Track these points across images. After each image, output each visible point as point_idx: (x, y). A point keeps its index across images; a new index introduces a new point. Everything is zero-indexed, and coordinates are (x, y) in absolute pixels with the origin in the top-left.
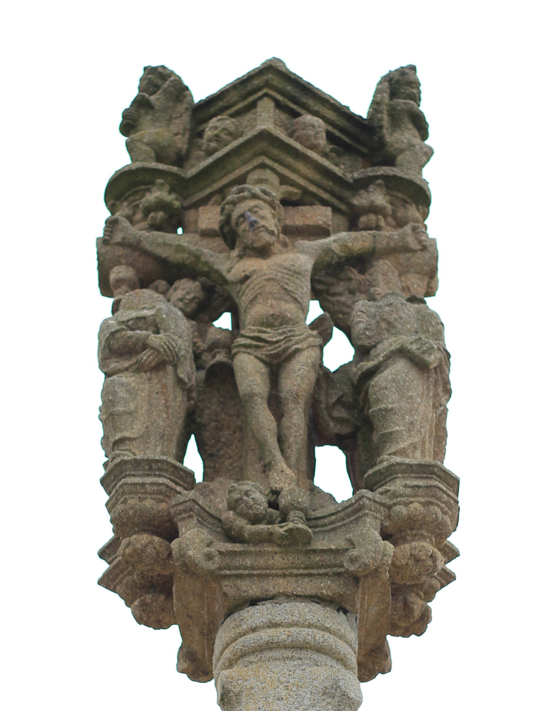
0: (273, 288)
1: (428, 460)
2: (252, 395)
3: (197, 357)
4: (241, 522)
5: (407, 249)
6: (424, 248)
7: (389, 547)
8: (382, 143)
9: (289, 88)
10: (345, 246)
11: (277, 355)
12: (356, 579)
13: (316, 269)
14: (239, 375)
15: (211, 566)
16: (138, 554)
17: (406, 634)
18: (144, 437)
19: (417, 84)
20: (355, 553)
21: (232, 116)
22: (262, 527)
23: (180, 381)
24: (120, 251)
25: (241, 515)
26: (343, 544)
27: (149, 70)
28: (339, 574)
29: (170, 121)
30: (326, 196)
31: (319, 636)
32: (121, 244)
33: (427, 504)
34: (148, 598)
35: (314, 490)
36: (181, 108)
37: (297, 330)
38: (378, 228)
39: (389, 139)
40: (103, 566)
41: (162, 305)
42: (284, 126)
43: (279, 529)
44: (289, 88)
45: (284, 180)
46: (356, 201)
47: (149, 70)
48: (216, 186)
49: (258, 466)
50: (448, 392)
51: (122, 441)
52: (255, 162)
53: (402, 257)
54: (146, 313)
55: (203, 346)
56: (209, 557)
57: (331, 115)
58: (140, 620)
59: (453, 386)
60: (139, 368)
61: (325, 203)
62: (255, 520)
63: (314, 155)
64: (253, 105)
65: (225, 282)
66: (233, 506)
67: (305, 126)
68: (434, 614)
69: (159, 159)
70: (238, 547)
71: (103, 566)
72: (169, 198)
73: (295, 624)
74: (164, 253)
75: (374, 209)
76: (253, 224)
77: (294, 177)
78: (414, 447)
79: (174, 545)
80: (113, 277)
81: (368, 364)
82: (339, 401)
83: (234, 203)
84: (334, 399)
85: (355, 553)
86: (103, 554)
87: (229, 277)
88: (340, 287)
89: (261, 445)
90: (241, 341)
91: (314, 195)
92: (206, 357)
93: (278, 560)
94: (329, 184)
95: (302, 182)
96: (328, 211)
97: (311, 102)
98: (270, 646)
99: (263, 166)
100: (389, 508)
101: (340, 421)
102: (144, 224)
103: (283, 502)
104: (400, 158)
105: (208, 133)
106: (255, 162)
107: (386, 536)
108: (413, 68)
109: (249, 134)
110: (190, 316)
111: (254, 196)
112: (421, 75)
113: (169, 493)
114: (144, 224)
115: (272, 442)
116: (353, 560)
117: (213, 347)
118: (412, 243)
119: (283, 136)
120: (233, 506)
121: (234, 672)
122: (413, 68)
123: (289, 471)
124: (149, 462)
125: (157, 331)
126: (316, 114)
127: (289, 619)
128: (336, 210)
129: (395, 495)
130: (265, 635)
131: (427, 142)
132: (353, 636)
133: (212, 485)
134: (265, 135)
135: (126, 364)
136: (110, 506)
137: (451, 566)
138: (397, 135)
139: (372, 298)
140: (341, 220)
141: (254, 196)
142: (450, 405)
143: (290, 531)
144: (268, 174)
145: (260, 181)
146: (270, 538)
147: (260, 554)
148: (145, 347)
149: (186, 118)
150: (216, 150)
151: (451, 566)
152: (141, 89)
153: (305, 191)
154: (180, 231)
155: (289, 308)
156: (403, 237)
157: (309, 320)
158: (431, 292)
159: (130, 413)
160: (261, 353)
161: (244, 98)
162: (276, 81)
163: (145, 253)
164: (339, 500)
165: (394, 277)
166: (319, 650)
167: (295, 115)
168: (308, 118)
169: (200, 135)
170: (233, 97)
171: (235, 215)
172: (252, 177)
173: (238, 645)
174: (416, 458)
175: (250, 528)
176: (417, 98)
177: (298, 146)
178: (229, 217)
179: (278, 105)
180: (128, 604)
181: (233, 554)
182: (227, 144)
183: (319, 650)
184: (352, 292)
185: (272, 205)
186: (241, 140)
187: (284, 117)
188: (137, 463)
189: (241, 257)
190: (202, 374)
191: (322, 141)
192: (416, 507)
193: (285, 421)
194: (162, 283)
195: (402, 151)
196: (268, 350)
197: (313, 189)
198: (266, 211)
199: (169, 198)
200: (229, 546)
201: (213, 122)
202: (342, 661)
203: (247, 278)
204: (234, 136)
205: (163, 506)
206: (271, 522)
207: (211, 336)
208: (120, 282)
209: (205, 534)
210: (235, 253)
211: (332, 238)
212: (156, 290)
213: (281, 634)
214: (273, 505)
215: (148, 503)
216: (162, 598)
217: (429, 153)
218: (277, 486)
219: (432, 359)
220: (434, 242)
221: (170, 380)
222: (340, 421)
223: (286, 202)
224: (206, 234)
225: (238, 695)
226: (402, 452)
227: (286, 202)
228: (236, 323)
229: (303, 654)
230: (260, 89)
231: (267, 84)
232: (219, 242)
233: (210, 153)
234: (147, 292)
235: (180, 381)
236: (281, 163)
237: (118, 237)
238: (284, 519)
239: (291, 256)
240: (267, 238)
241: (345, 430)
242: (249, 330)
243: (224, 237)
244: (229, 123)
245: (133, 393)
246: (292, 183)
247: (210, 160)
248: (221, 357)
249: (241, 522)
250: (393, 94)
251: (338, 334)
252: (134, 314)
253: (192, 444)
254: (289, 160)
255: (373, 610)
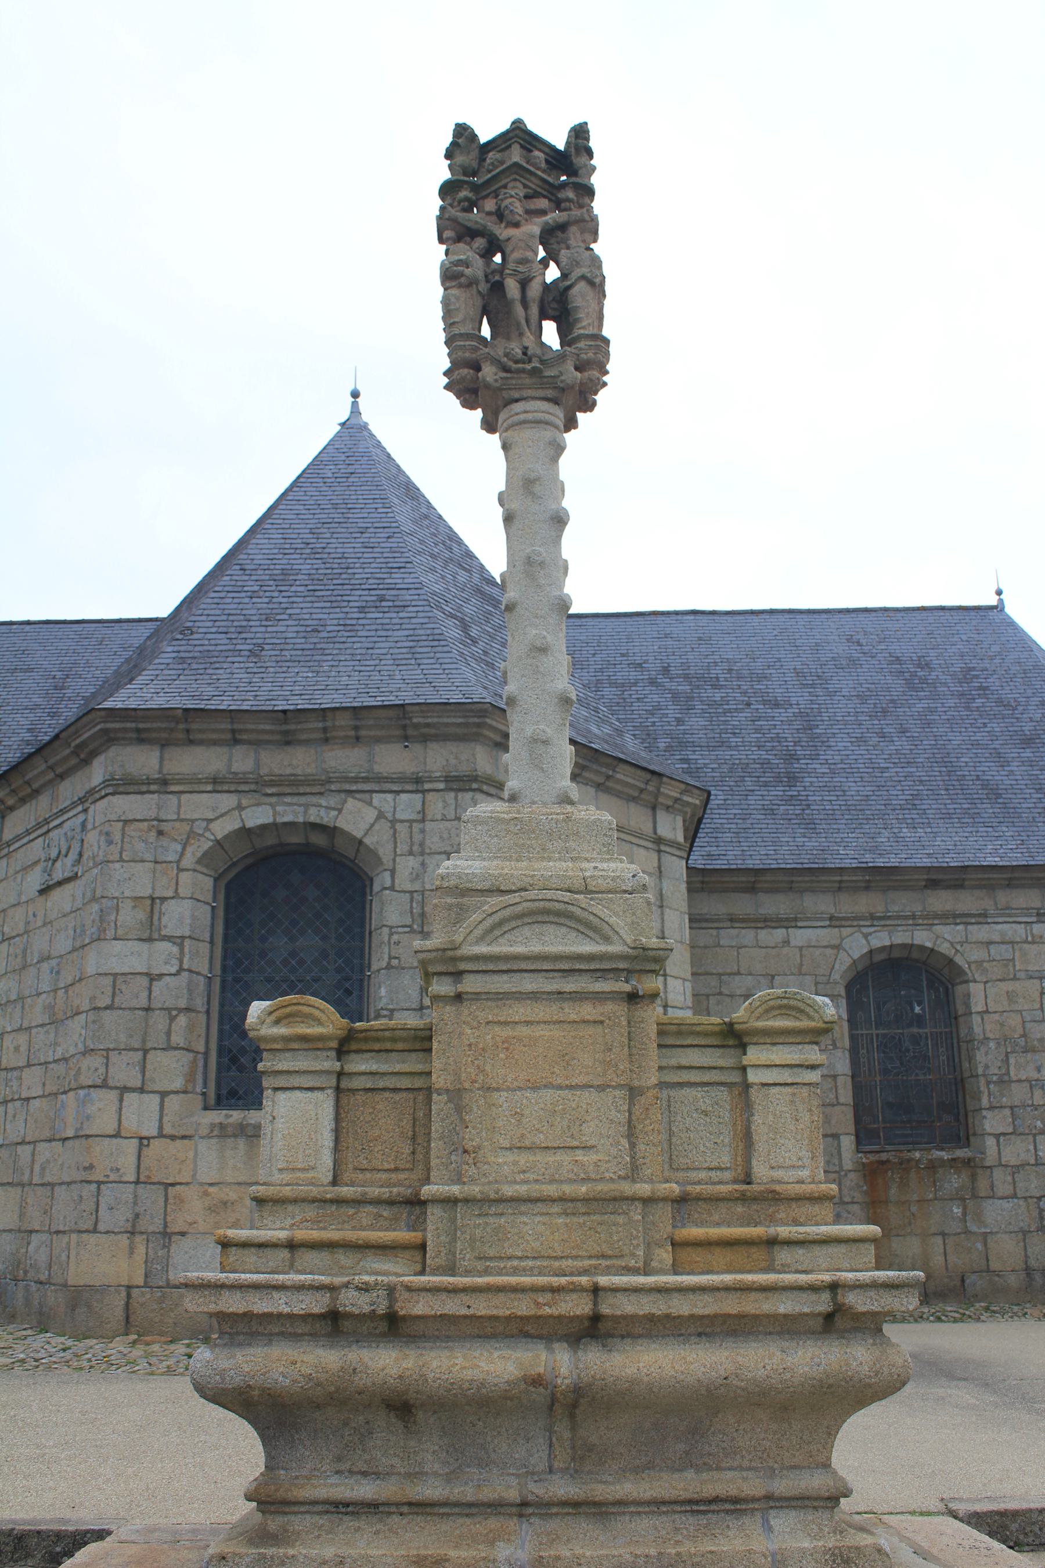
0: (523, 245)
1: (595, 332)
2: (513, 300)
3: (486, 276)
4: (510, 363)
5: (583, 220)
6: (592, 220)
7: (579, 375)
8: (571, 163)
9: (527, 137)
10: (555, 221)
11: (524, 279)
12: (563, 390)
13: (541, 232)
14: (507, 290)
15: (497, 385)
16: (463, 379)
17: (585, 411)
18: (463, 321)
19: (588, 132)
20: (562, 378)
21: (499, 151)
22: (520, 366)
23: (479, 292)
24: (448, 223)
25: (510, 359)
26: (557, 373)
27: (458, 125)
28: (555, 388)
29: (469, 153)
30: (545, 193)
31: (547, 417)
32: (448, 219)
33: (595, 354)
34: (467, 396)
35: (543, 344)
36: (474, 146)
37: (534, 266)
38: (570, 209)
39: (574, 161)
40: (446, 380)
41: (470, 254)
42: (525, 158)
43: (528, 367)
44: (527, 137)
45: (525, 186)
46: (559, 196)
47: (458, 125)
48: (493, 189)
49: (517, 333)
50: (604, 296)
51: (454, 323)
52: (512, 178)
53: (582, 224)
54: (462, 257)
55: (489, 271)
56: (496, 381)
57: (547, 150)
58: (463, 406)
59: (607, 293)
60: (460, 286)
61: (545, 197)
62: (516, 362)
63: (539, 173)
64: (510, 146)
65: (498, 239)
66: (506, 355)
67: (535, 157)
68: (598, 403)
69: (465, 174)
70: (509, 375)
71: (446, 380)
72: (470, 195)
73: (536, 411)
74: (469, 224)
75: (568, 200)
76: (511, 211)
77: (530, 184)
78: (589, 324)
79: (480, 374)
80: (444, 236)
81: (569, 283)
82: (554, 299)
83: (502, 200)
84: (551, 299)
85: (562, 378)
86: (446, 374)
87: (501, 238)
88: (553, 241)
89: (518, 324)
90: (507, 271)
91: (540, 193)
92: (490, 277)
93: (528, 381)
94: (547, 187)
95: (534, 187)
96: (546, 201)
97: (537, 144)
98: (525, 422)
99: (515, 180)
100: (578, 355)
101: (554, 309)
102: (458, 208)
103: (529, 353)
104: (580, 172)
105: (488, 161)
106: (512, 178)
107: (577, 369)
108: (586, 123)
109: (508, 164)
110: (482, 256)
111: (512, 196)
112: (590, 127)
113: (476, 349)
114: (458, 208)
115: (523, 322)
116: (562, 381)
117: (494, 272)
118: (587, 218)
119: (525, 165)
120: (506, 355)
121: (509, 433)
122: (586, 123)
123: (531, 337)
124: (467, 334)
125: (468, 267)
126: (540, 150)
127: (532, 409)
128: (550, 200)
129: (581, 349)
130: (522, 417)
131: (592, 162)
132: (562, 416)
133: (496, 342)
134: (516, 164)
135: (454, 284)
136: (449, 355)
137: (605, 378)
138: (578, 159)
139: (568, 248)
140: (553, 205)
141: (512, 196)
142: (605, 302)
143: (533, 368)
144: (518, 184)
145: (514, 188)
146: (523, 371)
147: (520, 378)
148: (462, 275)
149: (477, 151)
150: (492, 171)
151: (605, 378)
152: (454, 136)
153: (535, 191)
154: (475, 210)
155: (529, 254)
156: (582, 215)
157: (539, 258)
158: (595, 241)
159: (457, 309)
160: (517, 278)
161: (505, 142)
162: (521, 134)
163: (459, 224)
164: (484, 138)
165: (578, 235)
166: (547, 423)
167: (530, 151)
168: (537, 153)
169: (484, 160)
170: (499, 142)
171: (503, 205)
172: (510, 185)
173: (510, 421)
174: (590, 331)
175: (514, 366)
176: (588, 139)
177: (532, 169)
178: (500, 207)
179: (522, 146)
180: (458, 398)
181: (507, 378)
182: (497, 167)
183: (547, 423)
184: (558, 243)
185: (520, 200)
186: (504, 166)
187: (524, 152)
188: (461, 335)
189: (506, 227)
190: (489, 285)
191: (543, 165)
192: (591, 355)
193: (529, 312)
194: (468, 239)
195: (581, 168)
196: (521, 276)
197: (539, 190)
198: (518, 204)
199: (470, 195)
200: (505, 375)
201: (491, 154)
202: (557, 427)
203: (509, 239)
204: (502, 163)
205: (474, 355)
206: (524, 363)
207: (493, 267)
208: (448, 239)
209: (494, 369)
210: (503, 225)
211: (548, 217)
212: (465, 243)
213: (530, 416)
214: (525, 354)
215: (467, 355)
216: (473, 396)
217: (594, 169)
218: (526, 345)
219: (597, 281)
220: (597, 216)
221: (474, 292)
222: (554, 309)
223: (527, 197)
224: (489, 214)
225: (511, 445)
226: (583, 328)
227: (527, 197)
228: (503, 258)
229: (540, 425)
230: (512, 138)
231: (517, 136)
232: (494, 218)
233: (489, 171)
234: (461, 245)
235: (479, 292)
236: (522, 177)
237: (447, 216)
238: (530, 361)
239: (530, 227)
240: (518, 218)
241: (557, 313)
242: (511, 265)
243: (498, 216)
244: (498, 156)
245: (458, 299)
246: (529, 188)
247: (489, 176)
248: (497, 278)
249: (510, 363)
250: (577, 137)
251: (552, 264)
252: (456, 258)
253: (485, 319)
254: (528, 176)
255: (570, 402)
